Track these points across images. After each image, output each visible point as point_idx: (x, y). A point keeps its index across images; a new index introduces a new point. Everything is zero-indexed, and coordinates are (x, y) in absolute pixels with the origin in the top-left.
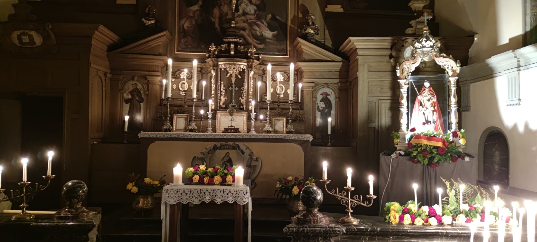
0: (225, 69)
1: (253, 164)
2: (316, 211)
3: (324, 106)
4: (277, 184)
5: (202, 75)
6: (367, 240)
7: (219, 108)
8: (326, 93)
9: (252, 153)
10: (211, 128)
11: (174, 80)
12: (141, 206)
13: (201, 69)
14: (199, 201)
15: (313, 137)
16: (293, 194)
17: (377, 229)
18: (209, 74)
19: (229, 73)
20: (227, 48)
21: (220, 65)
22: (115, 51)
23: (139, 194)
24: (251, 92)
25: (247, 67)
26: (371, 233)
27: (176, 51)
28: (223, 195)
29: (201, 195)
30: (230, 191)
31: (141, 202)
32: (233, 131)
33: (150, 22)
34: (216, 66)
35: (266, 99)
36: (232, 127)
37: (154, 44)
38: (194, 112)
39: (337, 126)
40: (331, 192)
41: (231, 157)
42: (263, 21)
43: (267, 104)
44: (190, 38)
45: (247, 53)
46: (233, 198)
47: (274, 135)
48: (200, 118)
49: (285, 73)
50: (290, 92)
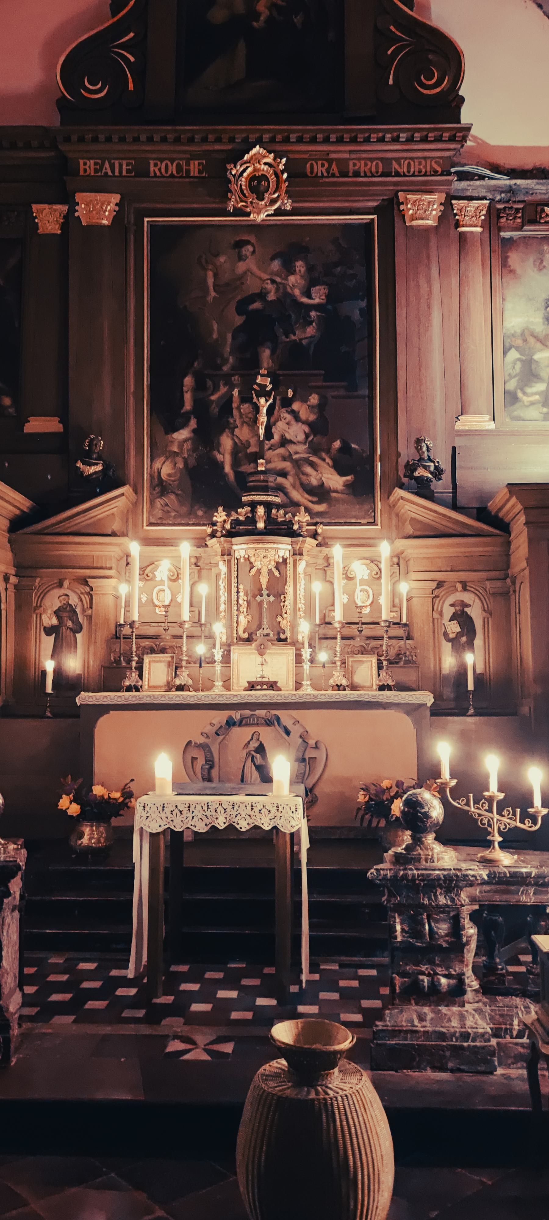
2: (430, 838)
3: (459, 629)
5: (199, 571)
7: (235, 641)
8: (462, 601)
14: (206, 825)
15: (434, 698)
18: (214, 571)
20: (250, 515)
22: (26, 530)
23: (83, 817)
24: (301, 605)
25: (292, 553)
27: (145, 524)
28: (252, 813)
29: (208, 813)
30: (264, 806)
32: (265, 687)
33: (92, 470)
34: (227, 553)
35: (334, 618)
36: (264, 680)
38: (185, 649)
39: (488, 671)
40: (459, 803)
42: (324, 455)
43: (336, 628)
44: (172, 497)
45: (291, 523)
50: (384, 601)
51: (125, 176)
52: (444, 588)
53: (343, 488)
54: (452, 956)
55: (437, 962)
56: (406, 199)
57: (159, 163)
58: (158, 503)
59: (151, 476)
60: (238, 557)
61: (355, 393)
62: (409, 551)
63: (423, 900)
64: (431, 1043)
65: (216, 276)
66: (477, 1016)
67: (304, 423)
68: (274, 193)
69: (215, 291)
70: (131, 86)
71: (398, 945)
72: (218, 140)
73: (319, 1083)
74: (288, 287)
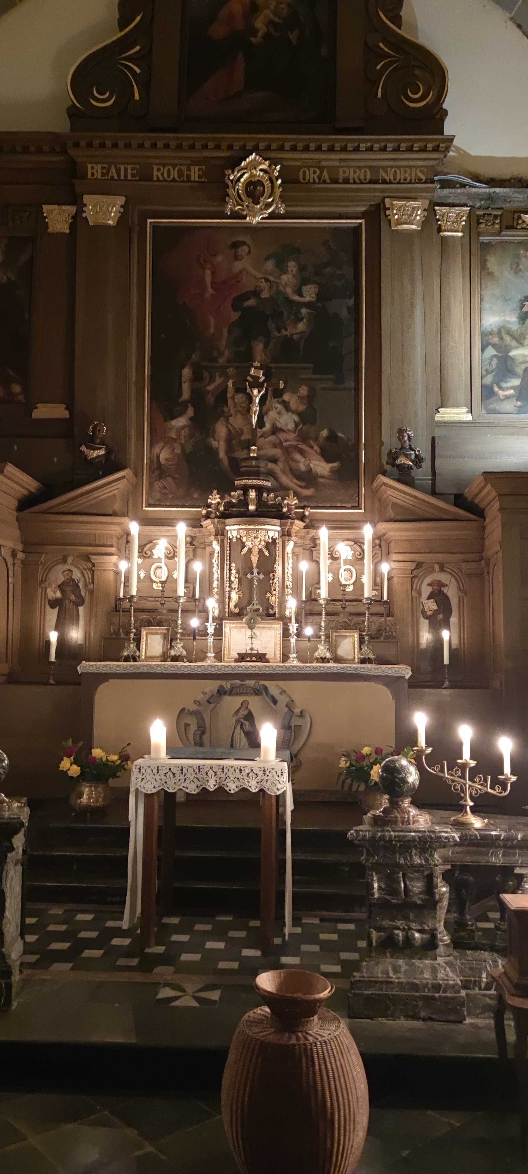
0: (239, 539)
1: (293, 724)
2: (406, 803)
3: (436, 608)
4: (341, 761)
5: (194, 550)
6: (500, 856)
7: (227, 615)
8: (440, 581)
9: (293, 701)
10: (214, 653)
11: (142, 560)
12: (86, 801)
13: (193, 538)
14: (197, 787)
15: (412, 671)
16: (372, 780)
17: (516, 836)
18: (208, 549)
19: (245, 546)
20: (242, 498)
21: (229, 532)
23: (83, 777)
24: (289, 583)
25: (281, 534)
26: (507, 844)
27: (144, 505)
28: (240, 777)
29: (199, 776)
30: (252, 770)
31: (85, 794)
32: (254, 659)
33: (95, 454)
34: (220, 533)
35: (319, 595)
36: (254, 652)
38: (180, 622)
39: (462, 647)
40: (434, 770)
41: (251, 710)
42: (312, 443)
43: (321, 605)
44: (170, 480)
45: (280, 506)
46: (258, 782)
47: (334, 667)
48: (194, 634)
49: (356, 543)
50: (366, 580)
55: (411, 918)
56: (392, 205)
57: (162, 168)
58: (157, 486)
59: (151, 461)
61: (342, 386)
64: (404, 993)
65: (213, 274)
66: (448, 969)
67: (294, 412)
68: (269, 198)
69: (212, 288)
70: (137, 96)
71: (375, 901)
72: (218, 147)
73: (300, 1029)
74: (280, 285)
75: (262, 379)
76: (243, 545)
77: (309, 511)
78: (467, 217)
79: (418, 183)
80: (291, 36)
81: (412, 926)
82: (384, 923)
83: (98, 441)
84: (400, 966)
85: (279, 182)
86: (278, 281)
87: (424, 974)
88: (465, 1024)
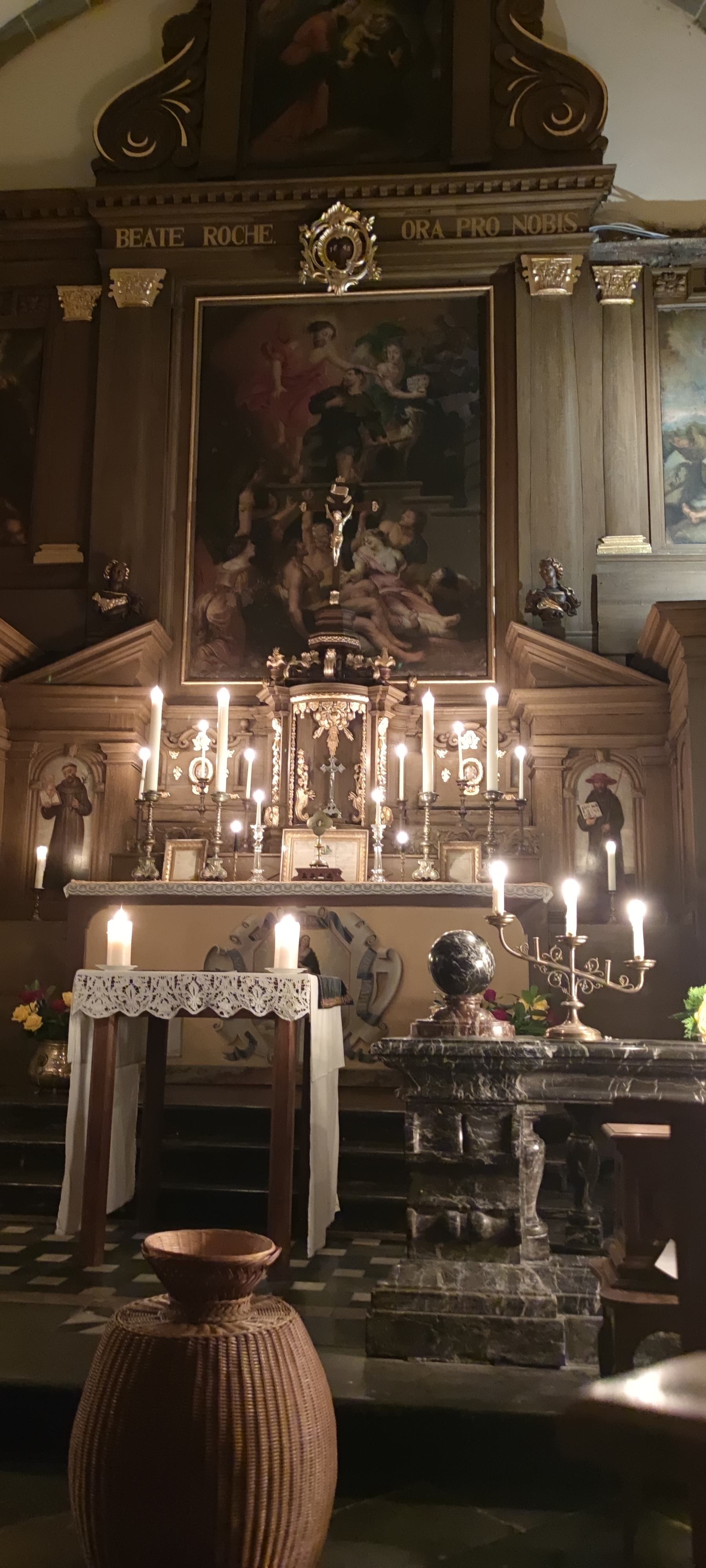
3: (599, 814)
6: (627, 1090)
8: (604, 775)
9: (375, 936)
11: (177, 754)
14: (172, 1009)
17: (651, 1053)
20: (317, 662)
21: (295, 706)
22: (22, 679)
25: (369, 708)
27: (183, 678)
28: (239, 992)
29: (176, 992)
33: (112, 604)
34: (283, 708)
37: (122, 658)
38: (219, 829)
41: (314, 950)
42: (420, 588)
43: (424, 802)
44: (220, 643)
45: (371, 670)
46: (265, 1001)
51: (171, 248)
52: (576, 758)
53: (446, 631)
54: (501, 1182)
55: (477, 1191)
56: (531, 263)
57: (215, 229)
58: (202, 652)
59: (193, 617)
60: (298, 713)
61: (463, 509)
62: (530, 707)
63: (457, 1091)
64: (460, 1316)
65: (284, 365)
66: (538, 1278)
67: (394, 548)
68: (359, 260)
69: (283, 384)
70: (184, 142)
71: (415, 1159)
72: (289, 197)
73: (210, 1319)
74: (377, 378)
75: (348, 499)
76: (317, 726)
77: (416, 682)
78: (639, 279)
79: (566, 233)
80: (392, 56)
81: (477, 1205)
82: (432, 1198)
83: (118, 587)
84: (456, 1271)
85: (374, 238)
86: (374, 372)
87: (495, 1284)
88: (563, 1371)
